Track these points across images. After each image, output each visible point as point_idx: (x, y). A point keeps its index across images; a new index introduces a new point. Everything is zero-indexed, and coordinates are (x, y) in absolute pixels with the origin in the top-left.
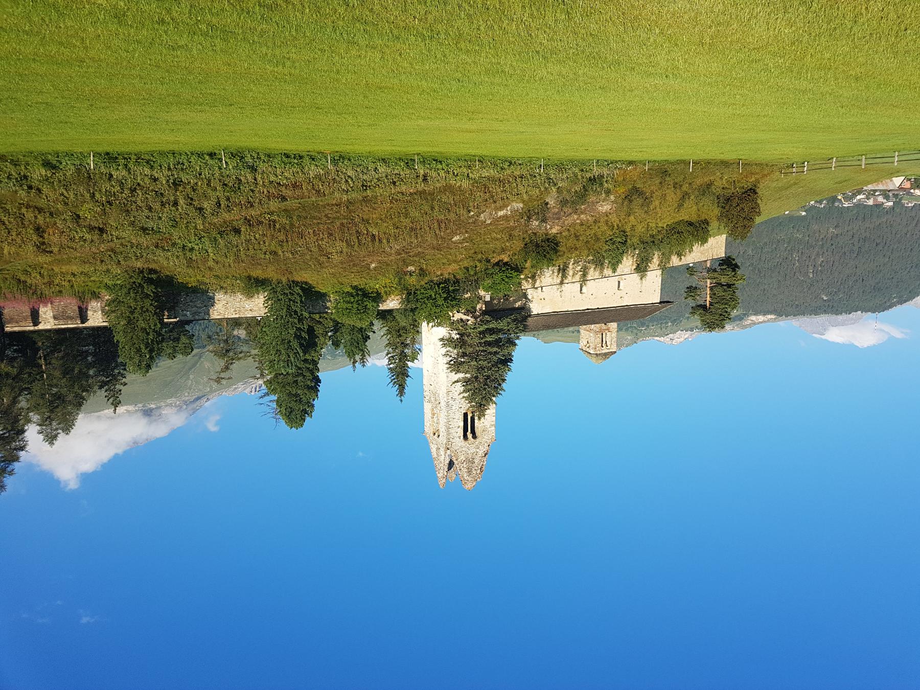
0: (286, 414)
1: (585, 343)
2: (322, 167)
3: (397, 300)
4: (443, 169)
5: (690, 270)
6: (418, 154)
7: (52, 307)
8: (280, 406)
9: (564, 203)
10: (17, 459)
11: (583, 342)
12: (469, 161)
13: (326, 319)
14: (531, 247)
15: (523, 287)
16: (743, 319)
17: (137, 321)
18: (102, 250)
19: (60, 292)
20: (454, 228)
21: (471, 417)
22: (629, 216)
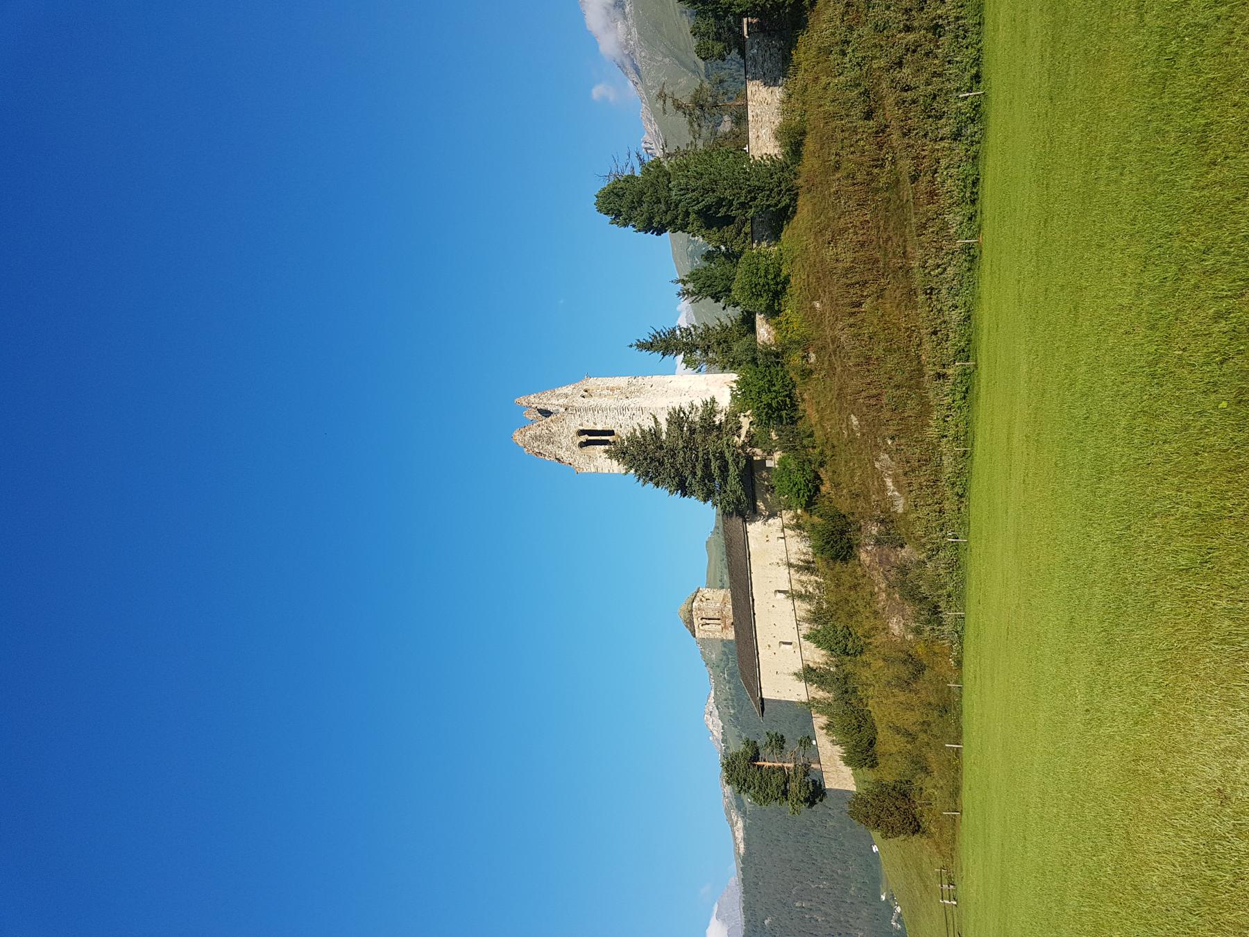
1: (707, 596)
2: (960, 232)
3: (769, 339)
4: (953, 401)
5: (807, 740)
6: (976, 366)
8: (626, 181)
9: (903, 570)
11: (707, 593)
12: (965, 438)
13: (744, 242)
14: (840, 524)
15: (784, 512)
22: (884, 660)
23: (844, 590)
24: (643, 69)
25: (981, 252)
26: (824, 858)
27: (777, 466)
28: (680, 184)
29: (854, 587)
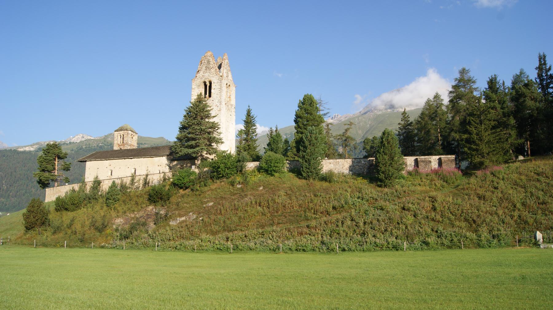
0: (314, 103)
1: (134, 138)
2: (285, 245)
3: (248, 168)
4: (216, 244)
5: (67, 181)
6: (230, 253)
7: (431, 167)
8: (316, 108)
9: (144, 224)
10: (454, 87)
11: (136, 138)
12: (201, 249)
13: (291, 157)
14: (165, 198)
15: (171, 173)
16: (38, 149)
17: (388, 159)
18: (404, 198)
19: (427, 176)
20: (212, 210)
21: (206, 94)
22: (104, 215)
23: (135, 199)
24: (366, 116)
25: (276, 253)
26: (17, 187)
27: (192, 170)
28: (313, 130)
29: (137, 203)
